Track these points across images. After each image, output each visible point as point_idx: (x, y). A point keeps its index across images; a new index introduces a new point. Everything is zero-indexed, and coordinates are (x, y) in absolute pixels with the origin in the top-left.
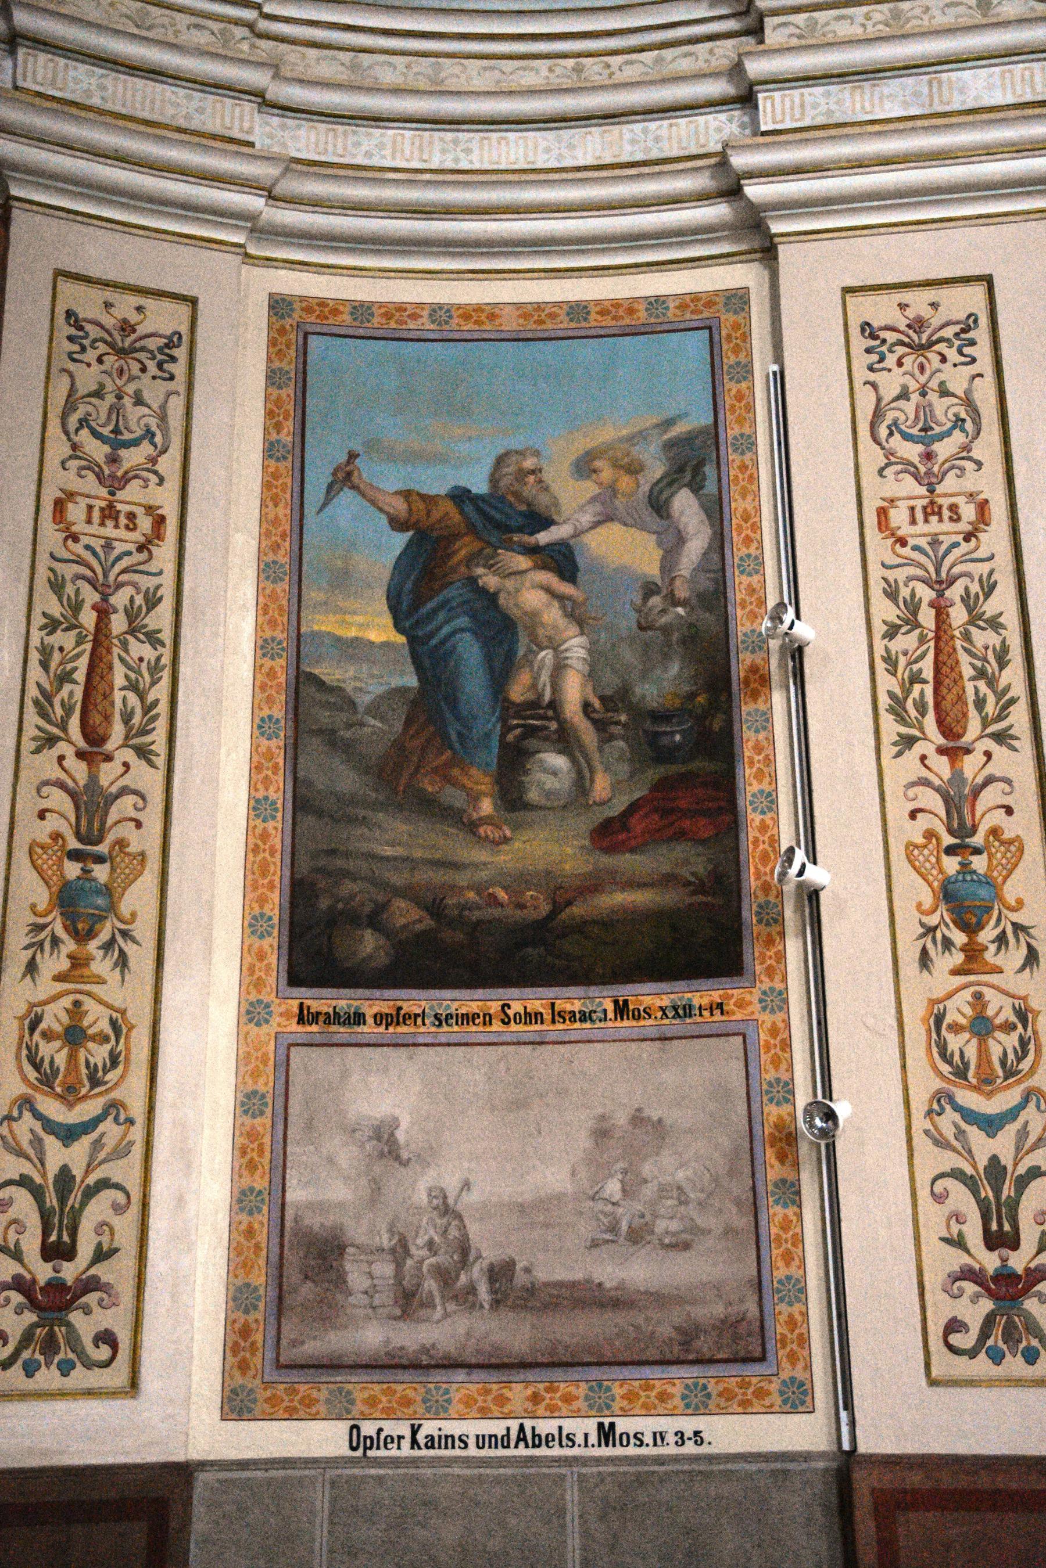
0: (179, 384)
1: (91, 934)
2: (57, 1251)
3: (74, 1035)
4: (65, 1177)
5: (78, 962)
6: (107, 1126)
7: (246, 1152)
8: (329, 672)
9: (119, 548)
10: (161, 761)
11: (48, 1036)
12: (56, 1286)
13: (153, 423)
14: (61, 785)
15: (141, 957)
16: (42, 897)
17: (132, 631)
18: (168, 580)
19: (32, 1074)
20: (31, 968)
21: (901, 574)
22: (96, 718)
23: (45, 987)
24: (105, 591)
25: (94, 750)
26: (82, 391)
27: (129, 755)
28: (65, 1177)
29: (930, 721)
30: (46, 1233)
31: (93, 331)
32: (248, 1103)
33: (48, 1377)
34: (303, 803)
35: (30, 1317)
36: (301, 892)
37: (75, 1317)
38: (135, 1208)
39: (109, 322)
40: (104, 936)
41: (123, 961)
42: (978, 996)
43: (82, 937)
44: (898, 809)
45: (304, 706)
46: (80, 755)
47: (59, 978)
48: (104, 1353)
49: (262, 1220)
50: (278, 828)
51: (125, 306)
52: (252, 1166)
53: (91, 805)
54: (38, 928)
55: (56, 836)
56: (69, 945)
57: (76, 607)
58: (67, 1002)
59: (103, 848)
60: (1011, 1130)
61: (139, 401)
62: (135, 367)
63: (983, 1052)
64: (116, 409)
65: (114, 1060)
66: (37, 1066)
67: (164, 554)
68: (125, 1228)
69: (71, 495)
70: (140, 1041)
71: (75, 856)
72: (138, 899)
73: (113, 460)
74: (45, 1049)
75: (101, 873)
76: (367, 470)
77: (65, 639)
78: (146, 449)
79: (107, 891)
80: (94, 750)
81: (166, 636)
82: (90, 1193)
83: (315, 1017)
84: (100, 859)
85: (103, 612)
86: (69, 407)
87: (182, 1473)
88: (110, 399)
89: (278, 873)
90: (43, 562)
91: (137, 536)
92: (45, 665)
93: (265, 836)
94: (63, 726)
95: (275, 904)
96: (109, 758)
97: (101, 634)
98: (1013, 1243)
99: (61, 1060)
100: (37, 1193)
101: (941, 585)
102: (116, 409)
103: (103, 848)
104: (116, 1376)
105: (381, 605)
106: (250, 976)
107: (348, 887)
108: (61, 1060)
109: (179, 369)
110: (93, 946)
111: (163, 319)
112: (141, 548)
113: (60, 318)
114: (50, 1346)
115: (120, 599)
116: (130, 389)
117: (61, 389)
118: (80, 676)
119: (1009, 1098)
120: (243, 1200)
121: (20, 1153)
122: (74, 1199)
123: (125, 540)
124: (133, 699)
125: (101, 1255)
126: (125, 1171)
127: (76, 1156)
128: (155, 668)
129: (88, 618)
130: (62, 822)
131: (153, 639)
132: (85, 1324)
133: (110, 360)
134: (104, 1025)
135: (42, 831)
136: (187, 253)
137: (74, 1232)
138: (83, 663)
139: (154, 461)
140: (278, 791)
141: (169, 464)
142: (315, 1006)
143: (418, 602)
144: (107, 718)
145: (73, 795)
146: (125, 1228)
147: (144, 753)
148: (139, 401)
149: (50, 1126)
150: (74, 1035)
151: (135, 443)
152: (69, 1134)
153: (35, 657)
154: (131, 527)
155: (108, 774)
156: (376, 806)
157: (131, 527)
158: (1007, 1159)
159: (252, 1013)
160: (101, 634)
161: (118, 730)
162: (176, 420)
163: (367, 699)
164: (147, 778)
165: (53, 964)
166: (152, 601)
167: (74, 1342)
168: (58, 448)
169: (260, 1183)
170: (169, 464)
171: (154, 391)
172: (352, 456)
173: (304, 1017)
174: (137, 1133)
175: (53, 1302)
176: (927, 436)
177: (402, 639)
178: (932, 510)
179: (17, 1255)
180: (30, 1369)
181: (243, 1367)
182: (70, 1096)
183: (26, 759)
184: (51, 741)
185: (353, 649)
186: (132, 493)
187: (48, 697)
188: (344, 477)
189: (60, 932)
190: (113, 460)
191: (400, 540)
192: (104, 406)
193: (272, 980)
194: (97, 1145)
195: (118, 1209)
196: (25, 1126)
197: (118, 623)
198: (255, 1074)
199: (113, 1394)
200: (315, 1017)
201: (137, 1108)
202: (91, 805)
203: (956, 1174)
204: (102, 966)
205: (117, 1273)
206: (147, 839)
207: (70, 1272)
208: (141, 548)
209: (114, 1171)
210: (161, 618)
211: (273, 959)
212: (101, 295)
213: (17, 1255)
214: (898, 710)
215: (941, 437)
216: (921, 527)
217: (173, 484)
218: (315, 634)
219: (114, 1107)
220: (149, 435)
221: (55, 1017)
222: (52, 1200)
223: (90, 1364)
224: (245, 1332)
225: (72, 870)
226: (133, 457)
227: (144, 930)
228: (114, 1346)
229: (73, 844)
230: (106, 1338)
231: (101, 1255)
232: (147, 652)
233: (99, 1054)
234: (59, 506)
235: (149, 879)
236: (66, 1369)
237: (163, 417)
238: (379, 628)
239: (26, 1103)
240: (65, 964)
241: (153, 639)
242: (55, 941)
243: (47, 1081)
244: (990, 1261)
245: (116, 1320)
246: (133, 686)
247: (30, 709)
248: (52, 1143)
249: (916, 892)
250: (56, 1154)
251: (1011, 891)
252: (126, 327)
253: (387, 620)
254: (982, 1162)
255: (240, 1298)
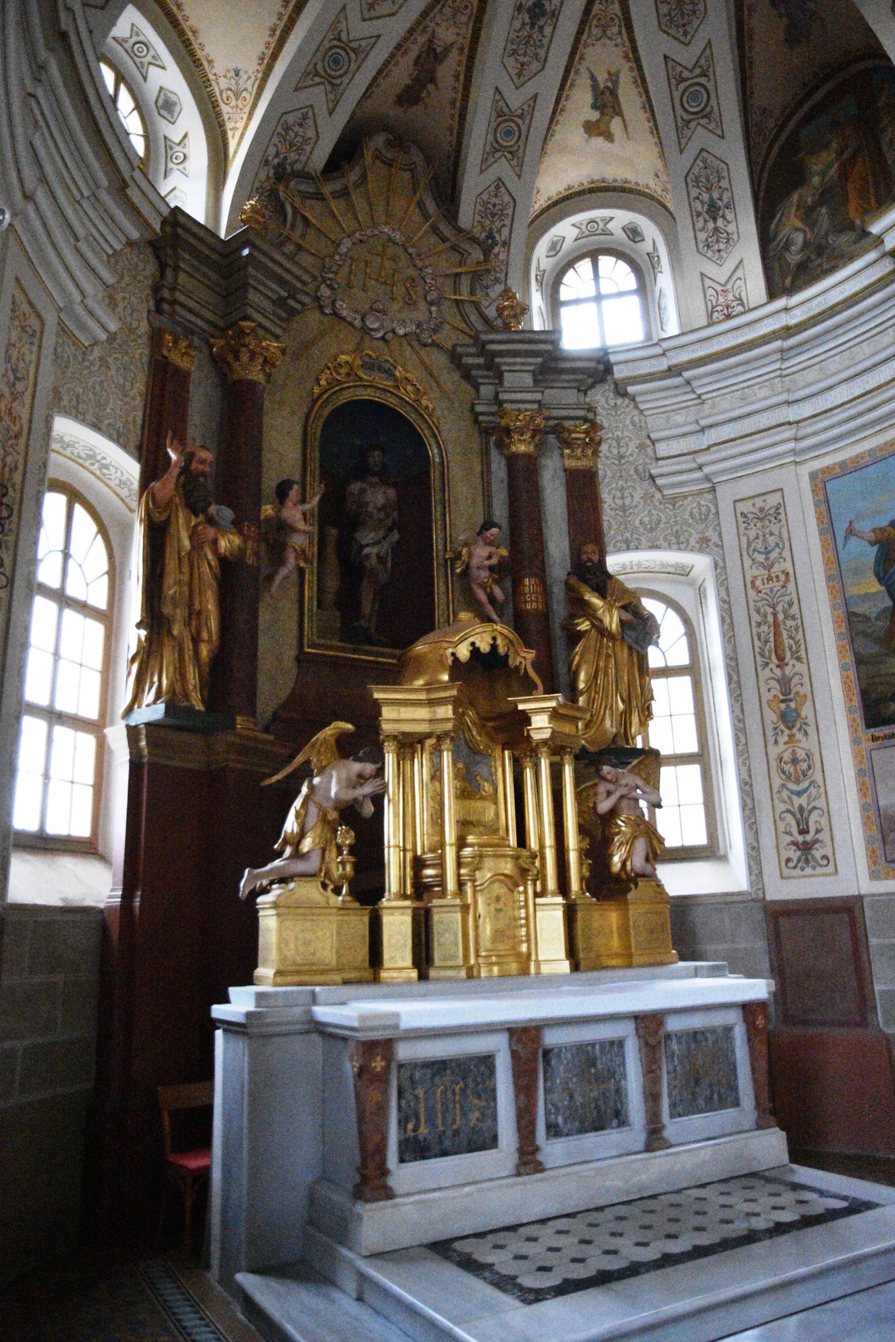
0: (784, 521)
1: (793, 727)
2: (803, 832)
3: (795, 761)
4: (801, 808)
5: (791, 736)
6: (812, 789)
7: (862, 790)
8: (858, 609)
9: (775, 590)
10: (805, 661)
11: (786, 763)
12: (805, 843)
13: (777, 540)
14: (774, 679)
15: (811, 730)
16: (774, 718)
17: (786, 618)
18: (794, 596)
19: (784, 777)
20: (776, 742)
21: (760, 604)
22: (779, 652)
23: (782, 747)
24: (773, 607)
25: (782, 662)
26: (751, 539)
27: (794, 661)
28: (801, 808)
29: (773, 657)
30: (798, 825)
31: (750, 516)
32: (860, 773)
33: (808, 871)
34: (860, 661)
35: (799, 853)
36: (864, 693)
37: (814, 852)
38: (826, 814)
39: (756, 511)
40: (798, 726)
41: (806, 734)
42: (794, 751)
43: (790, 728)
44: (763, 689)
45: (853, 624)
46: (778, 666)
47: (786, 743)
48: (825, 862)
49: (872, 813)
50: (852, 674)
51: (759, 502)
52: (865, 795)
53: (785, 684)
54: (776, 728)
55: (775, 696)
56: (787, 732)
57: (765, 616)
58: (790, 750)
59: (791, 696)
60: (805, 795)
61: (771, 534)
62: (767, 522)
63: (796, 771)
64: (764, 540)
65: (810, 767)
66: (784, 773)
67: (791, 586)
68: (824, 821)
69: (756, 577)
70: (817, 758)
71: (783, 701)
72: (806, 711)
73: (767, 559)
74: (786, 768)
75: (793, 705)
76: (857, 526)
77: (764, 628)
78: (777, 550)
79: (796, 710)
80: (782, 662)
81: (798, 616)
82: (811, 811)
83: (878, 738)
84: (791, 700)
85: (775, 615)
86: (749, 544)
87: (860, 898)
88: (761, 538)
89: (856, 691)
90: (752, 604)
91: (781, 583)
92: (759, 639)
93: (848, 677)
94: (770, 658)
95: (856, 701)
96: (787, 664)
97: (776, 624)
98: (807, 832)
99: (792, 770)
100: (794, 815)
101: (773, 607)
102: (764, 540)
103: (791, 696)
104: (830, 869)
105: (874, 578)
106: (853, 729)
107: (881, 688)
108: (792, 770)
109: (782, 517)
110: (795, 731)
111: (773, 500)
112: (783, 587)
113: (739, 515)
114: (807, 861)
115: (779, 608)
116: (767, 531)
117: (744, 541)
118: (772, 639)
119: (805, 784)
120: (864, 808)
121: (785, 802)
122: (805, 815)
123: (776, 585)
124: (791, 642)
125: (818, 831)
126: (821, 803)
127: (803, 801)
128: (797, 629)
129: (770, 618)
130: (776, 691)
131: (793, 618)
132: (817, 853)
133: (759, 524)
134: (804, 756)
135: (770, 696)
136: (773, 474)
137: (807, 823)
138: (772, 635)
139: (780, 554)
140: (850, 659)
141: (786, 553)
142: (877, 734)
143: (886, 573)
144: (783, 650)
145: (778, 681)
146: (824, 821)
147: (799, 659)
148: (771, 534)
149: (793, 792)
150: (795, 761)
151: (773, 550)
152: (799, 794)
153: (755, 638)
154: (778, 581)
155: (788, 670)
156: (887, 655)
157: (778, 581)
158: (805, 805)
159: (856, 742)
160: (776, 624)
161: (788, 655)
162: (785, 536)
163: (875, 615)
164: (800, 667)
165: (783, 739)
166: (790, 604)
167: (816, 861)
168: (748, 562)
169: (869, 800)
170: (786, 553)
171: (774, 528)
172: (850, 523)
173: (874, 739)
174: (822, 790)
175: (806, 848)
176: (767, 552)
177: (883, 588)
178: (770, 579)
179: (791, 835)
180: (803, 869)
181: (875, 863)
182: (798, 782)
183: (760, 674)
184: (767, 664)
185: (866, 597)
186: (776, 569)
187: (763, 650)
188: (850, 532)
189: (783, 728)
190: (767, 559)
191: (876, 548)
192: (760, 541)
193: (860, 728)
194: (809, 797)
195: (821, 816)
196: (785, 793)
197: (781, 617)
198: (861, 763)
199: (830, 875)
200: (878, 738)
201: (821, 783)
202: (785, 684)
203: (788, 811)
204: (799, 736)
205: (824, 836)
206: (803, 690)
207: (809, 838)
208: (783, 587)
209: (816, 804)
210: (794, 610)
211: (859, 720)
212: (751, 502)
213: (791, 835)
214: (762, 655)
215: (770, 552)
216: (767, 586)
217: (789, 560)
218: (851, 597)
219: (813, 782)
220: (777, 545)
221: (787, 756)
222: (798, 816)
223: (821, 866)
224: (873, 851)
225: (783, 706)
226: (774, 555)
227: (811, 720)
228: (828, 860)
229: (781, 697)
230: (825, 857)
231: (818, 831)
232: (793, 623)
233: (804, 766)
234: (753, 583)
235: (809, 703)
236: (814, 868)
237: (780, 537)
238: (875, 587)
239: (783, 786)
240: (787, 738)
241: (793, 618)
242: (782, 731)
243: (789, 778)
244: (800, 839)
245: (828, 851)
246: (791, 637)
247: (758, 656)
248: (794, 797)
249: (771, 717)
250: (797, 801)
251: (803, 714)
252: (762, 510)
253: (876, 582)
254: (796, 806)
255: (869, 840)
